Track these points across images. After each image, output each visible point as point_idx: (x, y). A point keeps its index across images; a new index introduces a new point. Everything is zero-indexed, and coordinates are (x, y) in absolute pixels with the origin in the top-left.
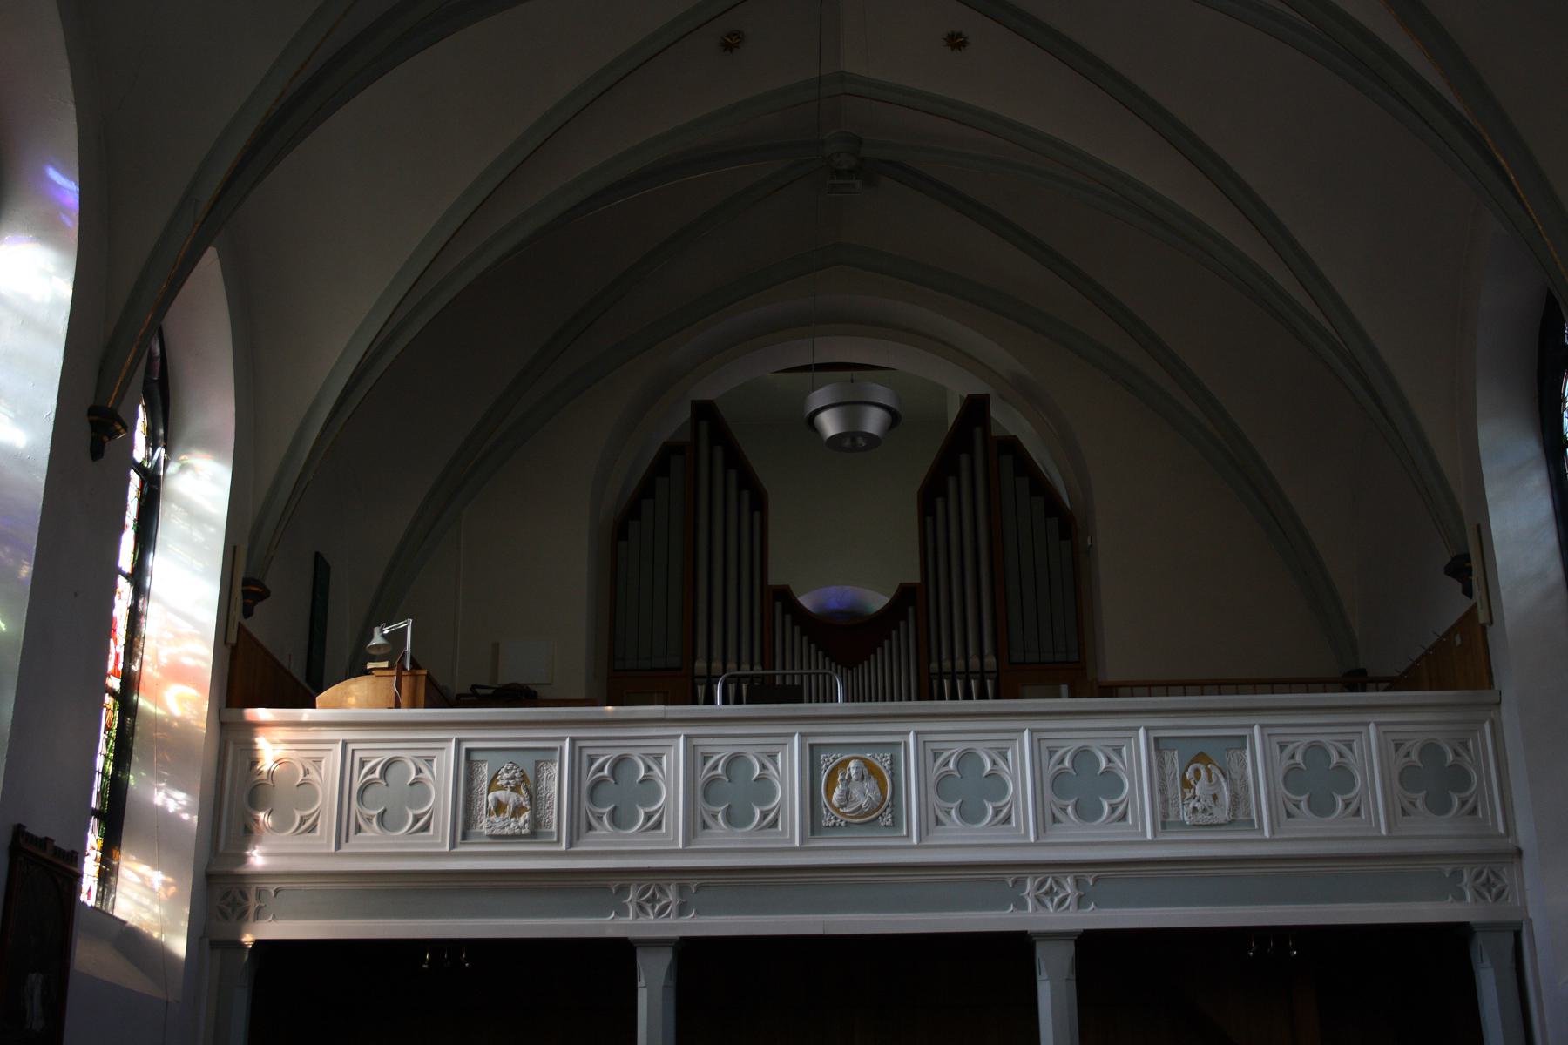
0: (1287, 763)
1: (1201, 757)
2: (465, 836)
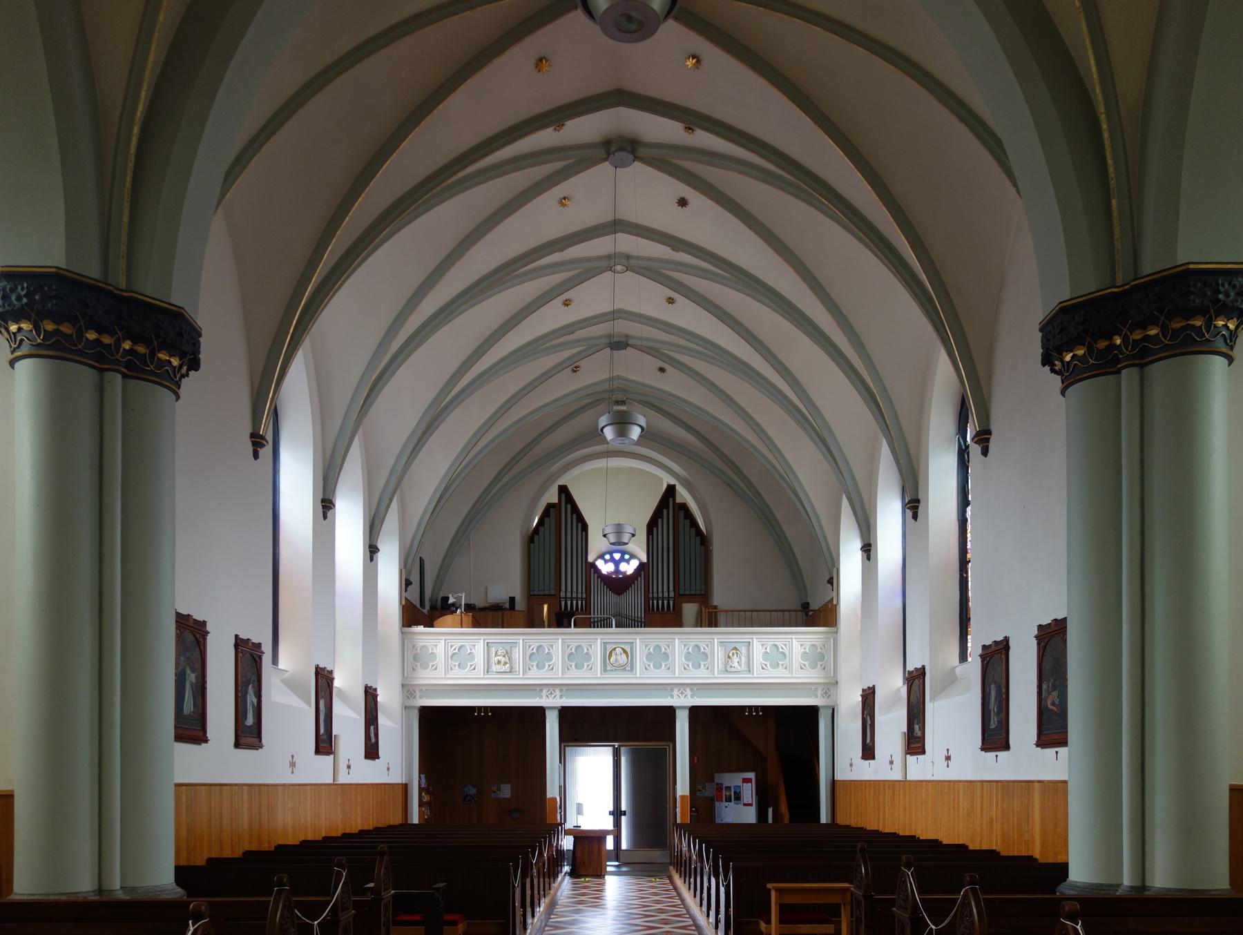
1: (735, 648)
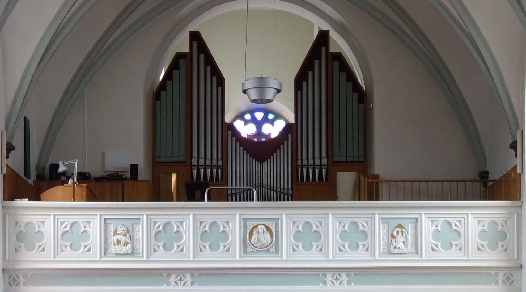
0: (434, 228)
2: (105, 254)
